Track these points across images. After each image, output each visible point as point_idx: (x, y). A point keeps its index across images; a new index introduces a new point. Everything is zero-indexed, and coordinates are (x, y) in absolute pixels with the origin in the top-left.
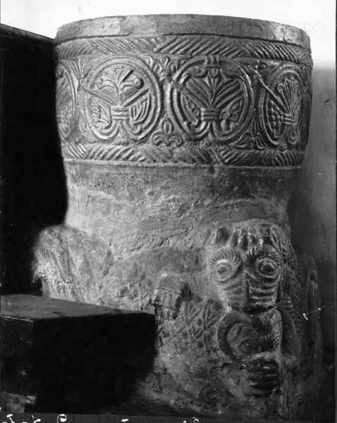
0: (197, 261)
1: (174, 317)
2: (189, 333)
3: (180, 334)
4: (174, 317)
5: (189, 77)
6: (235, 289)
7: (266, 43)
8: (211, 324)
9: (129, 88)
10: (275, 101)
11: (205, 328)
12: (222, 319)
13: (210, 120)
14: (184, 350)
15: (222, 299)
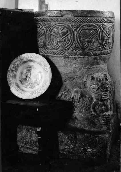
0: (85, 85)
1: (79, 102)
2: (83, 107)
3: (81, 107)
4: (79, 102)
5: (82, 30)
6: (97, 94)
7: (104, 18)
8: (90, 104)
9: (64, 33)
10: (106, 35)
11: (88, 105)
12: (93, 103)
13: (88, 43)
14: (82, 112)
15: (93, 97)
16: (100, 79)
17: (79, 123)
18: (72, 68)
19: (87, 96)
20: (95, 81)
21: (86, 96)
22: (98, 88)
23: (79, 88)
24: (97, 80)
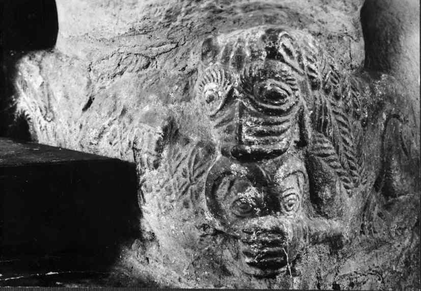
1: (156, 166)
4: (156, 166)
6: (225, 127)
16: (239, 51)
17: (161, 259)
18: (138, 10)
19: (195, 139)
20: (218, 63)
21: (191, 137)
22: (230, 98)
23: (160, 103)
24: (226, 59)
